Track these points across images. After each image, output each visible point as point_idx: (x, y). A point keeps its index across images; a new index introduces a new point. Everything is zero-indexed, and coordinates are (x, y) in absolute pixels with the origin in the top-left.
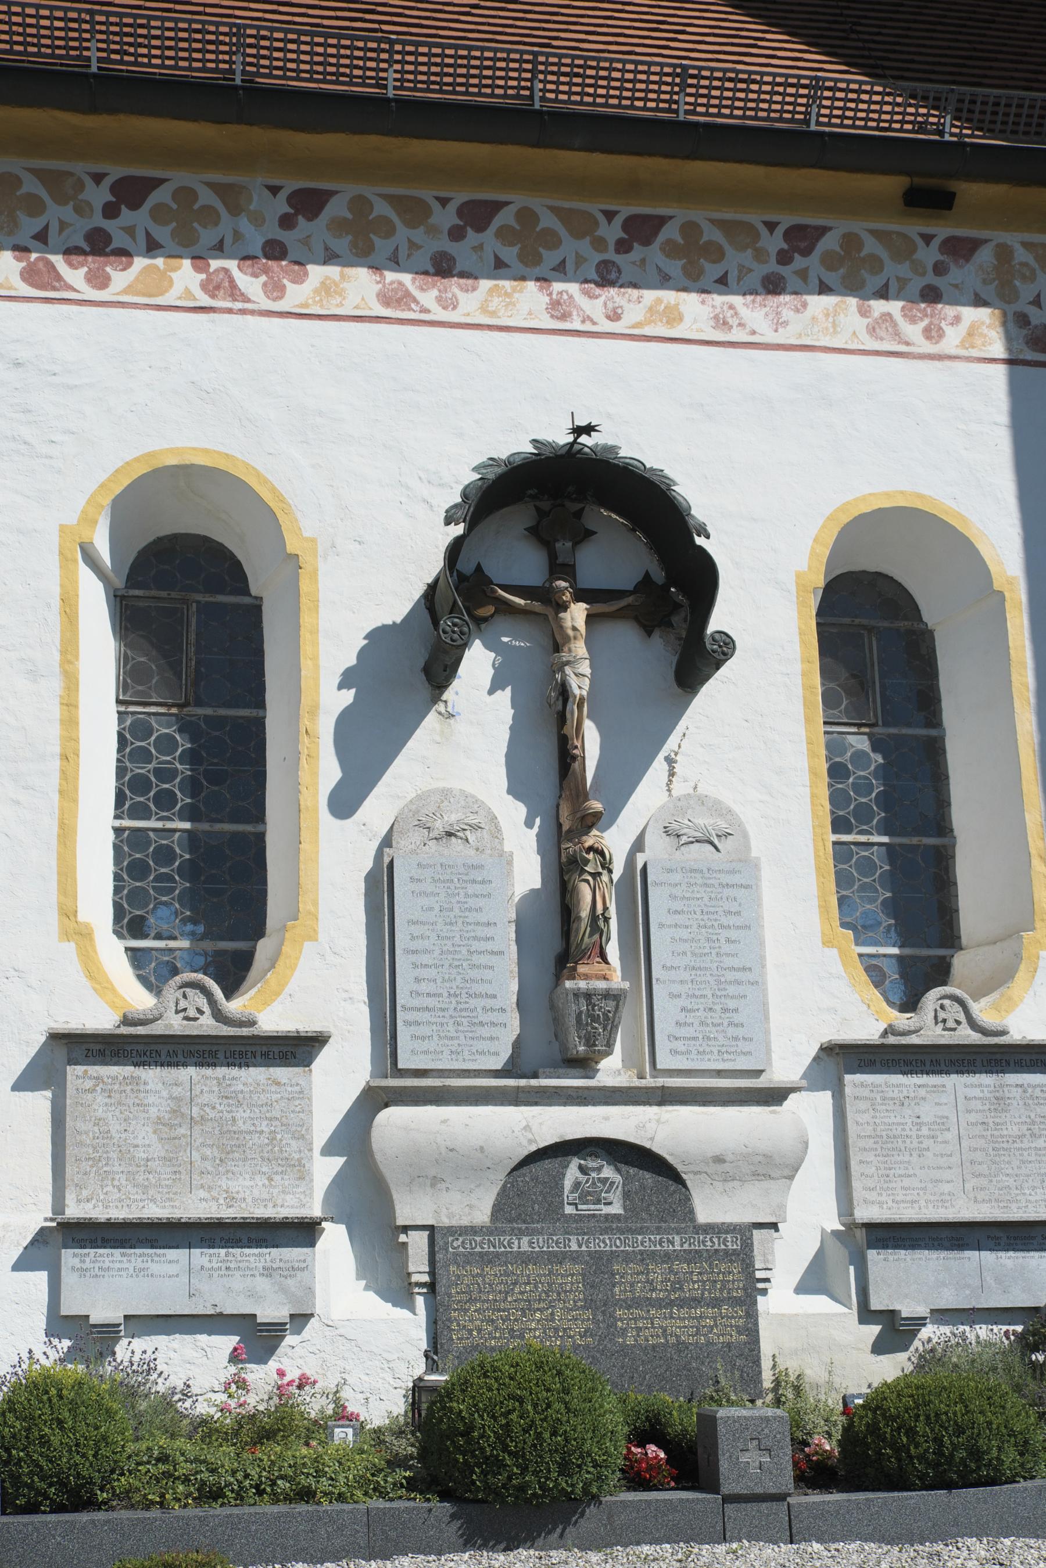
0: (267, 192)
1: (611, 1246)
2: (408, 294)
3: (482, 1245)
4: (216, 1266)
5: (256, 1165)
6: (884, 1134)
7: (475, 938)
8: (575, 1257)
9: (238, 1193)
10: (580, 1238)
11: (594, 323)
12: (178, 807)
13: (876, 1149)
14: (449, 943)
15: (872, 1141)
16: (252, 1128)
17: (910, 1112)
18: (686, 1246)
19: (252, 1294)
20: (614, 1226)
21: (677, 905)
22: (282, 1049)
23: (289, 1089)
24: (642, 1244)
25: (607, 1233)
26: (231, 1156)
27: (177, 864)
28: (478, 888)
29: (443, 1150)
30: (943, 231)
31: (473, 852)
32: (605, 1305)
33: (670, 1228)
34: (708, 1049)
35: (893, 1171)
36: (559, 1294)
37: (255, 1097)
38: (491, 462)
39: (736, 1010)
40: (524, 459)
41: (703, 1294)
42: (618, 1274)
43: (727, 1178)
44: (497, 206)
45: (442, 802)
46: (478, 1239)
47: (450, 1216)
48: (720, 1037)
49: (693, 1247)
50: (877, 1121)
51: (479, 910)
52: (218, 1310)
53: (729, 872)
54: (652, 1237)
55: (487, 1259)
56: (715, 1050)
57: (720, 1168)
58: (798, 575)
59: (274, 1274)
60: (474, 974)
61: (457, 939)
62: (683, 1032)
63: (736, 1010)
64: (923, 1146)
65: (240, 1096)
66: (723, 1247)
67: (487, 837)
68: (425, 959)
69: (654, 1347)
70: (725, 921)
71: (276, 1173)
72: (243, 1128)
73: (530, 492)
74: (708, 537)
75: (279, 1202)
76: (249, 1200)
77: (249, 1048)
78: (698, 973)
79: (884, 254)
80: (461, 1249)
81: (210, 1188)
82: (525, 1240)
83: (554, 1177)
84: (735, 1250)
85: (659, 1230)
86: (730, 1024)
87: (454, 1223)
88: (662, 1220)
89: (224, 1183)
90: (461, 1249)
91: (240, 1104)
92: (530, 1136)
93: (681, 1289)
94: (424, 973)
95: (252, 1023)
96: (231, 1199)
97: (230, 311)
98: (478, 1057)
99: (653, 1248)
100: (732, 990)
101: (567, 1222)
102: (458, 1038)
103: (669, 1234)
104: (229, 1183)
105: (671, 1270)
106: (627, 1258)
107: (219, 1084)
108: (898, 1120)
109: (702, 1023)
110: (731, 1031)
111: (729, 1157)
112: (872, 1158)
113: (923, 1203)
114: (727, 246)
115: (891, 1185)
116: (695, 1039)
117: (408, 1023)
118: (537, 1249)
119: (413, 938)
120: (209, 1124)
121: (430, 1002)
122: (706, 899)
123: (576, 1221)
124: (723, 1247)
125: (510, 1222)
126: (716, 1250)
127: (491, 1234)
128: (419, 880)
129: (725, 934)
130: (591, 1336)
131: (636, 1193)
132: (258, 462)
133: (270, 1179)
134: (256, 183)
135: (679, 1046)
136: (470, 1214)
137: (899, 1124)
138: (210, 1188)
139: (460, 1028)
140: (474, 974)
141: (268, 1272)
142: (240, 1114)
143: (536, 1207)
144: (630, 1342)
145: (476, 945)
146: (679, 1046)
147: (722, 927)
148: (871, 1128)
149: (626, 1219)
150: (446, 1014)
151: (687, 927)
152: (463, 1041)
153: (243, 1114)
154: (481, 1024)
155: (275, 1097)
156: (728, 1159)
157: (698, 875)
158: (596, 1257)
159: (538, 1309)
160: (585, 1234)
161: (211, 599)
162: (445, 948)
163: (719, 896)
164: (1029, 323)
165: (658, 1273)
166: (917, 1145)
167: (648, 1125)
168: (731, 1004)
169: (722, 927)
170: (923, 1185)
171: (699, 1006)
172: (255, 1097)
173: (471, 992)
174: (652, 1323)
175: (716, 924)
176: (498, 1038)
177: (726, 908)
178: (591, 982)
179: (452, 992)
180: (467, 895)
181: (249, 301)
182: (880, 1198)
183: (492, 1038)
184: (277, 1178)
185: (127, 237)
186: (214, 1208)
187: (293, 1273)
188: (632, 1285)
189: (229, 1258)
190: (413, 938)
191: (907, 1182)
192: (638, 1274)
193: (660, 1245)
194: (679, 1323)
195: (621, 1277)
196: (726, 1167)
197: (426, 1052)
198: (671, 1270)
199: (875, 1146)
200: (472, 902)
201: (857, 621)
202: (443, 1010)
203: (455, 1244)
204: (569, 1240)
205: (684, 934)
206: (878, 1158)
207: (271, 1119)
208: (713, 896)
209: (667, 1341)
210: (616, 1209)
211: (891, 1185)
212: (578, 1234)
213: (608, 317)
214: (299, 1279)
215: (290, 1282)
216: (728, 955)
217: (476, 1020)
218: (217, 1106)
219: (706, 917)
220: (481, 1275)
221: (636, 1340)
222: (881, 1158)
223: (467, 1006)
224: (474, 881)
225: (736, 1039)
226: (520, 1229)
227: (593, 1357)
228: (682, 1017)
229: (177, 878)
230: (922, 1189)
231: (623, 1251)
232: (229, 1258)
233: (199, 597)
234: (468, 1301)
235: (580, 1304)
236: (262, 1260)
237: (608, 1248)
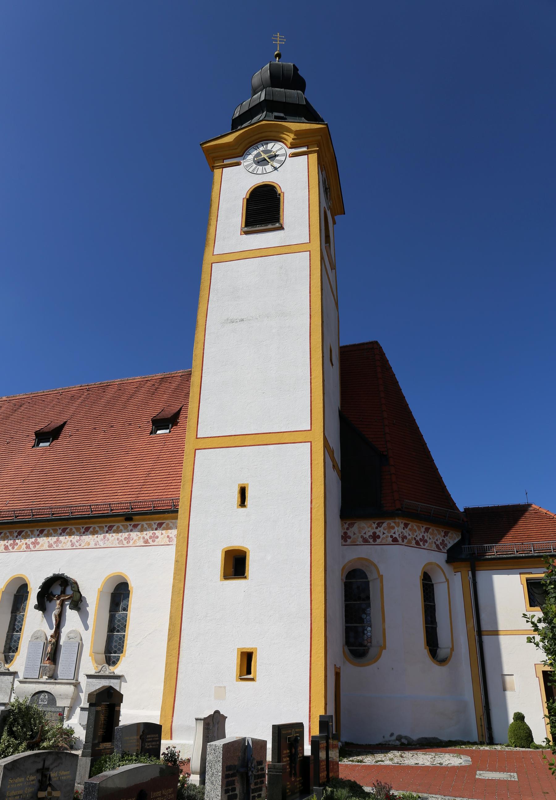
0: (37, 531)
2: (52, 545)
11: (77, 547)
30: (133, 523)
31: (40, 641)
39: (71, 668)
43: (62, 698)
44: (90, 527)
48: (68, 673)
58: (99, 589)
62: (62, 672)
63: (71, 668)
79: (123, 529)
85: (51, 707)
91: (3, 683)
97: (28, 551)
100: (71, 665)
110: (69, 672)
114: (99, 531)
116: (64, 673)
119: (29, 656)
134: (35, 529)
142: (3, 685)
164: (144, 538)
168: (70, 667)
169: (72, 653)
181: (149, 543)
185: (364, 533)
210: (46, 703)
213: (79, 546)
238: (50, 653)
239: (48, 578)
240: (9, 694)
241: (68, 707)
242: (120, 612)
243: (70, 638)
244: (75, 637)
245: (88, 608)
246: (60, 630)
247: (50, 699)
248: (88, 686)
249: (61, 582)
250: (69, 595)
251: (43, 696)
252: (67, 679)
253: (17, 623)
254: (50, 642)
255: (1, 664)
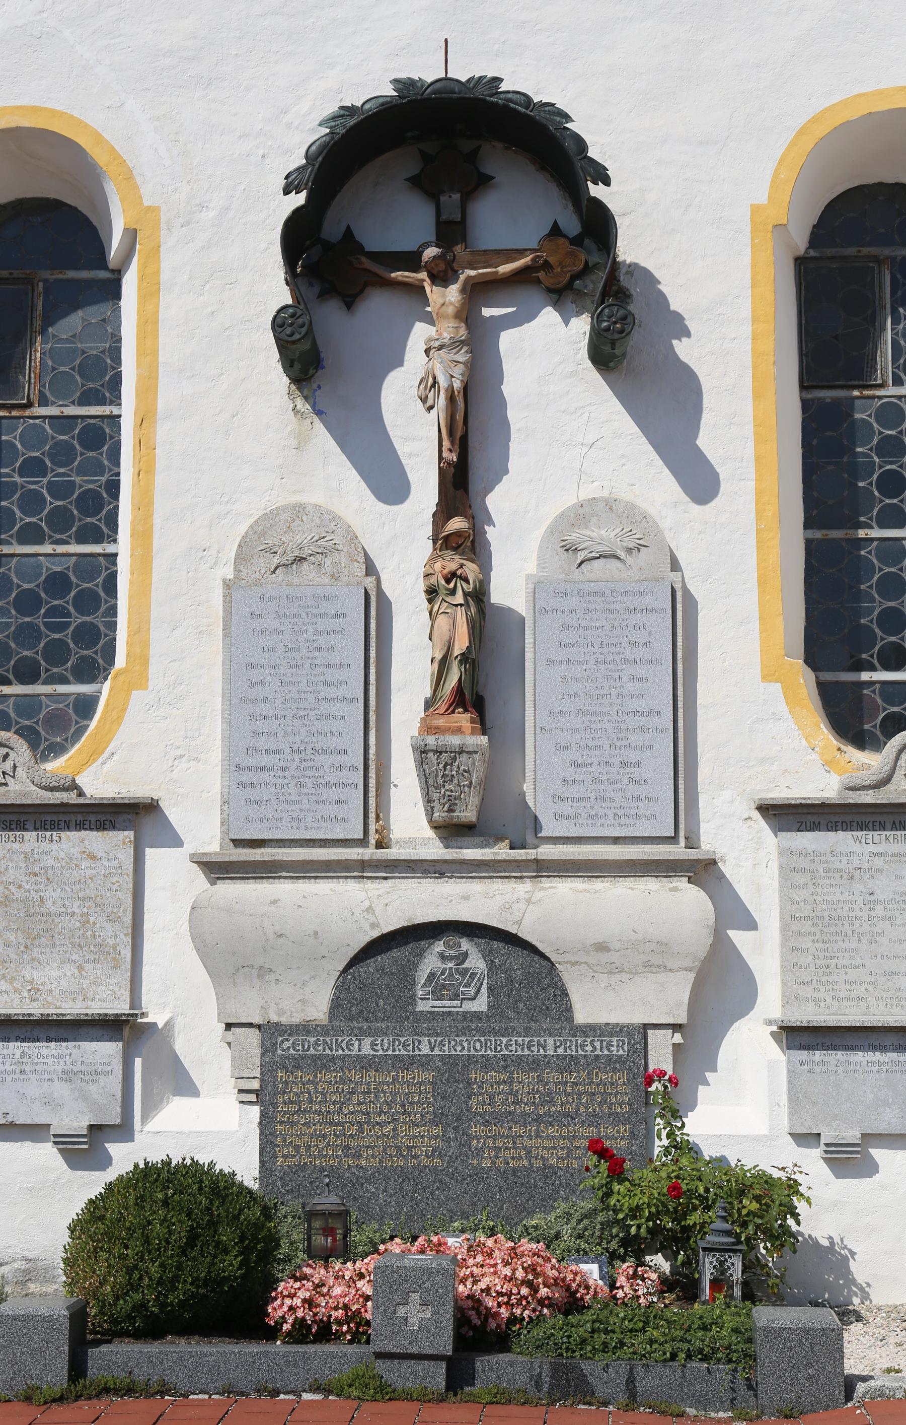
1: (469, 1050)
3: (315, 1047)
4: (9, 1068)
5: (66, 952)
6: (826, 914)
7: (324, 683)
8: (425, 1062)
9: (43, 984)
10: (433, 1040)
12: (16, 528)
13: (815, 934)
14: (294, 689)
15: (810, 923)
16: (63, 910)
17: (861, 888)
18: (561, 1051)
19: (48, 1102)
20: (473, 1026)
21: (572, 636)
22: (99, 817)
23: (106, 864)
24: (506, 1048)
25: (464, 1034)
26: (37, 942)
27: (13, 595)
28: (329, 623)
29: (271, 936)
31: (327, 580)
32: (458, 1120)
33: (541, 1028)
34: (601, 812)
35: (834, 961)
36: (403, 1106)
37: (67, 873)
38: (342, 112)
39: (639, 764)
40: (382, 104)
41: (578, 1109)
42: (476, 1083)
43: (613, 970)
45: (294, 521)
46: (312, 1039)
47: (281, 1012)
49: (569, 1052)
50: (818, 898)
51: (330, 649)
52: (10, 1120)
53: (638, 593)
54: (520, 1040)
55: (321, 1063)
56: (610, 813)
57: (604, 957)
58: (755, 210)
59: (74, 1078)
60: (321, 726)
61: (303, 686)
62: (573, 791)
63: (639, 764)
64: (877, 929)
65: (50, 872)
66: (606, 1052)
67: (344, 560)
68: (265, 709)
69: (514, 1171)
70: (629, 654)
71: (88, 961)
72: (53, 909)
73: (409, 134)
74: (607, 182)
75: (90, 995)
76: (56, 993)
77: (63, 818)
78: (594, 718)
80: (292, 1051)
81: (12, 980)
82: (367, 1041)
83: (403, 968)
84: (620, 1056)
85: (527, 1032)
86: (631, 780)
87: (284, 1020)
88: (532, 1019)
89: (28, 973)
90: (292, 1051)
92: (372, 919)
93: (552, 1102)
94: (263, 726)
95: (74, 786)
96: (35, 991)
98: (323, 824)
99: (520, 1053)
100: (634, 739)
101: (417, 1021)
102: (299, 802)
103: (540, 1036)
104: (35, 973)
105: (540, 1080)
106: (487, 1064)
107: (26, 858)
108: (846, 897)
109: (595, 780)
110: (632, 790)
111: (614, 945)
112: (810, 944)
113: (871, 1001)
115: (831, 979)
117: (354, 768)
118: (381, 1052)
120: (15, 905)
121: (269, 760)
122: (607, 627)
123: (428, 1020)
124: (606, 1052)
125: (350, 1020)
126: (597, 1057)
127: (327, 1034)
128: (261, 616)
129: (628, 670)
130: (440, 1156)
131: (502, 987)
132: (96, 118)
133: (81, 968)
135: (567, 808)
136: (302, 1010)
137: (845, 902)
138: (12, 980)
139: (304, 790)
140: (321, 726)
141: (68, 1076)
142: (52, 894)
143: (381, 1002)
144: (486, 1164)
145: (326, 692)
146: (567, 808)
147: (625, 661)
148: (809, 907)
149: (489, 1017)
150: (286, 773)
151: (581, 663)
152: (305, 806)
153: (54, 894)
154: (329, 785)
155: (89, 873)
156: (612, 946)
157: (599, 599)
158: (450, 1062)
159: (378, 1124)
160: (438, 1035)
161: (60, 276)
162: (289, 696)
163: (624, 623)
165: (525, 1081)
166: (869, 928)
167: (515, 906)
168: (633, 756)
169: (625, 661)
170: (873, 979)
171: (593, 760)
172: (67, 873)
173: (317, 747)
174: (514, 1143)
175: (618, 658)
176: (347, 802)
177: (633, 639)
178: (442, 738)
179: (295, 747)
180: (317, 632)
182: (816, 995)
183: (339, 802)
184: (88, 967)
186: (16, 1002)
187: (95, 1077)
188: (492, 1096)
189: (25, 1060)
190: (252, 685)
191: (852, 975)
192: (499, 1083)
193: (529, 1049)
194: (546, 1143)
195: (479, 1087)
196: (613, 957)
197: (262, 820)
198: (540, 1080)
199: (813, 930)
200: (322, 641)
201: (865, 251)
202: (284, 769)
203: (287, 1045)
204: (420, 1042)
205: (578, 671)
206: (817, 945)
207: (84, 899)
208: (616, 624)
209: (531, 1165)
210: (481, 1005)
211: (831, 979)
212: (429, 1035)
214: (102, 1084)
215: (93, 1088)
216: (632, 696)
217: (320, 781)
218: (24, 884)
219: (606, 650)
220: (312, 1082)
221: (493, 1163)
222: (820, 945)
223: (311, 764)
224: (325, 615)
225: (636, 799)
226: (360, 1029)
227: (441, 1181)
228: (570, 773)
229: (13, 612)
230: (871, 983)
231: (483, 1056)
232: (25, 1060)
233: (46, 274)
234: (295, 1113)
235: (428, 1118)
236: (62, 1062)
237: (465, 1052)
238: (464, 658)
239: (349, 111)
240: (127, 954)
241: (676, 1027)
242: (882, 386)
243: (581, 556)
244: (629, 550)
245: (683, 349)
246: (475, 501)
247: (510, 980)
248: (801, 879)
249: (425, 157)
250: (519, 253)
251: (443, 957)
252: (616, 840)
253: (17, 479)
254: (448, 581)
255: (4, 751)
